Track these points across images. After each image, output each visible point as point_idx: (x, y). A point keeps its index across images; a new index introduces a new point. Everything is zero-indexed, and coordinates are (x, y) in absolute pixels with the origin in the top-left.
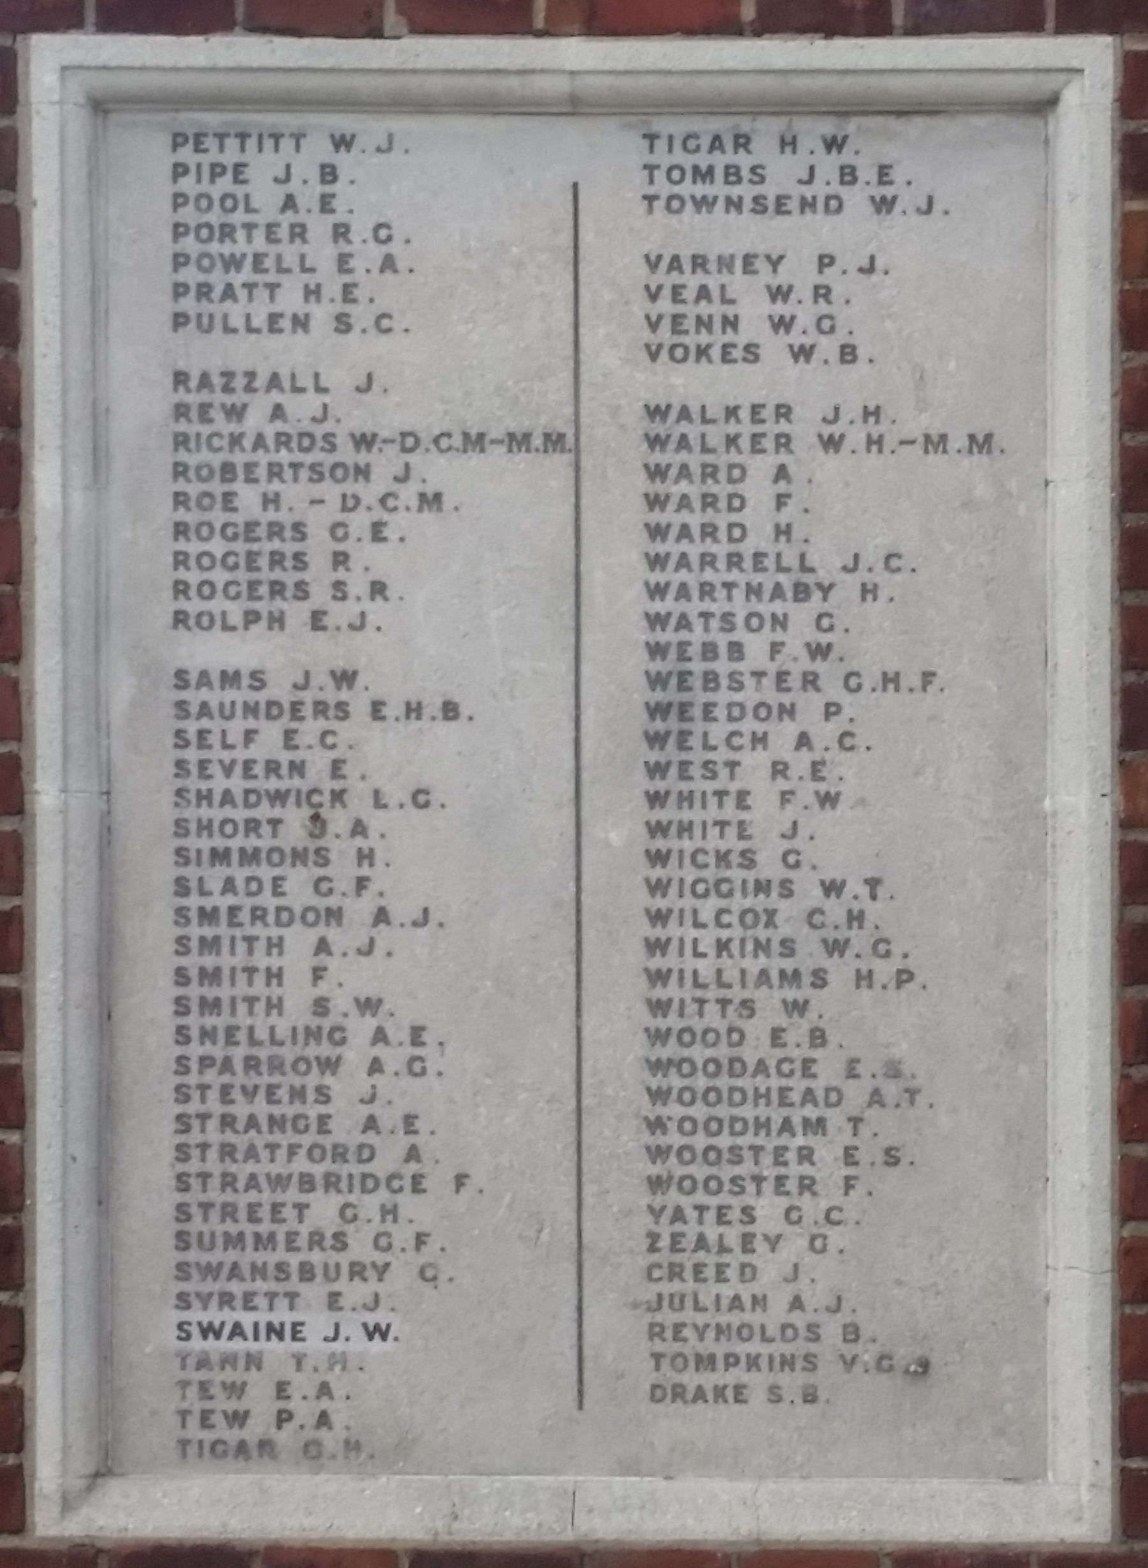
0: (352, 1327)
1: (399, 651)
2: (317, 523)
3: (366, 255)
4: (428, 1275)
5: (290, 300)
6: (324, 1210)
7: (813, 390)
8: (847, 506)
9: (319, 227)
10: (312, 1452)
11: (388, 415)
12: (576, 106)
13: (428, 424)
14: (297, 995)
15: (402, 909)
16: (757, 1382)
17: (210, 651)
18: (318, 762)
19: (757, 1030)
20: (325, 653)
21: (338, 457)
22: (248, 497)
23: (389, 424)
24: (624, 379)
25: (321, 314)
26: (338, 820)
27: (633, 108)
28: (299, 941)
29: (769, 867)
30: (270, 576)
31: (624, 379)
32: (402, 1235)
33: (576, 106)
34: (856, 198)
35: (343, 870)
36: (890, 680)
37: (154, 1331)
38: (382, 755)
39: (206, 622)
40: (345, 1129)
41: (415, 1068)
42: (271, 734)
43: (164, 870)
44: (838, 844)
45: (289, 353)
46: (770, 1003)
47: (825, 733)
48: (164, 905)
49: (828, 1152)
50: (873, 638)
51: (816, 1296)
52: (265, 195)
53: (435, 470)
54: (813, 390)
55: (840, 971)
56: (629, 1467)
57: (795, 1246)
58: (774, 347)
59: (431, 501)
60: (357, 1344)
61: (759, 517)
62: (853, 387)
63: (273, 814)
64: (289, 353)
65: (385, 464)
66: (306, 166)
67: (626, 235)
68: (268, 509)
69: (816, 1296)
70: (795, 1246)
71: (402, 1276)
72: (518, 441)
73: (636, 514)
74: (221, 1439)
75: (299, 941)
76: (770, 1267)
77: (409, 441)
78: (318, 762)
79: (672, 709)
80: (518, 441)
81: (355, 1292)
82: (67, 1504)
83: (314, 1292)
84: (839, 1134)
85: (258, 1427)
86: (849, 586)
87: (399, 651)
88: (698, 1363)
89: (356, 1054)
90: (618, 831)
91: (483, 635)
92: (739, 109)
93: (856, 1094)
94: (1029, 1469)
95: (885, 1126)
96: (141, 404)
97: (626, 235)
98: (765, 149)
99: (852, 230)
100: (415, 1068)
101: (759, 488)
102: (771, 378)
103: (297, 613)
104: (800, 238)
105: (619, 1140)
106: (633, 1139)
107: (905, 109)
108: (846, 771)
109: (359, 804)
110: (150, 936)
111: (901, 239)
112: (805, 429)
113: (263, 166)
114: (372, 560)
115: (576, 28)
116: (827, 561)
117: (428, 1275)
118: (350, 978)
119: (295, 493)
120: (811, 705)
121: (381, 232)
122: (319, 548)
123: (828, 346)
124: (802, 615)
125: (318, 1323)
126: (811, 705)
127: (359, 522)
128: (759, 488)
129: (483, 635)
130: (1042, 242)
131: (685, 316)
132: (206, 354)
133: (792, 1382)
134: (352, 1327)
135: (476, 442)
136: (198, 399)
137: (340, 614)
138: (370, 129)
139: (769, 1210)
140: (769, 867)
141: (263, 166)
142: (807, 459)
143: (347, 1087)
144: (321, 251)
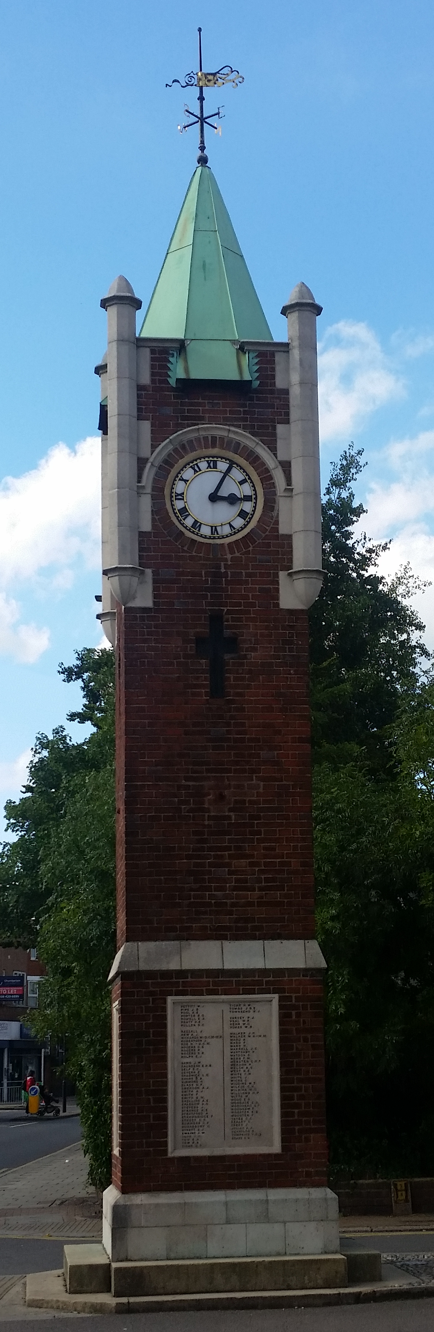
0: (201, 1132)
1: (205, 1060)
2: (196, 1046)
3: (201, 1018)
4: (208, 1126)
5: (193, 1023)
6: (198, 1120)
7: (247, 1031)
8: (251, 1043)
9: (196, 1015)
10: (197, 1147)
11: (204, 1035)
12: (223, 1002)
13: (208, 1036)
14: (195, 1096)
15: (206, 1087)
16: (243, 1137)
17: (185, 1060)
18: (197, 1072)
19: (243, 1099)
20: (197, 1060)
21: (199, 1039)
22: (189, 1044)
23: (204, 1035)
24: (228, 1030)
25: (197, 1024)
26: (199, 1078)
27: (229, 1002)
28: (195, 1091)
29: (244, 1081)
30: (191, 1052)
31: (228, 1030)
32: (206, 1122)
33: (223, 1002)
34: (252, 1011)
35: (199, 1083)
36: (256, 1061)
37: (180, 1133)
38: (203, 1070)
39: (185, 1057)
40: (200, 1111)
41: (207, 1104)
42: (191, 1069)
43: (181, 1084)
44: (251, 1079)
45: (194, 1028)
46: (244, 1096)
47: (249, 1067)
48: (181, 1088)
49: (250, 1111)
50: (254, 1057)
51: (249, 1128)
52: (191, 1012)
53: (209, 1040)
54: (247, 1031)
55: (251, 1092)
56: (230, 1147)
57: (247, 1122)
58: (243, 1027)
59: (208, 1044)
60: (201, 1134)
61: (242, 1044)
62: (252, 1030)
63: (192, 1077)
64: (194, 1028)
65: (203, 1040)
66: (195, 1009)
67: (228, 1015)
68: (191, 1045)
69: (249, 1128)
70: (247, 1122)
71: (206, 1127)
72: (217, 1037)
73: (230, 1044)
74: (187, 1145)
75: (195, 1091)
76: (244, 1124)
77: (206, 1037)
78: (197, 1072)
79: (233, 1065)
80: (217, 1037)
81: (201, 1129)
82: (172, 1153)
83: (196, 1129)
84: (251, 1110)
85: (191, 1143)
86: (251, 1051)
87: (205, 1060)
88: (237, 1135)
89: (201, 1103)
90: (228, 1078)
91: (213, 1057)
92: (239, 1002)
93: (253, 1106)
94: (271, 1145)
95: (256, 1109)
96: (178, 1034)
97: (228, 1015)
98: (242, 1006)
99: (251, 1014)
100: (207, 1104)
101: (242, 1041)
102: (243, 1030)
103: (194, 1056)
104: (246, 1015)
105: (228, 1110)
106: (230, 1111)
107: (205, 1002)
108: (251, 1071)
109: (201, 1076)
110: (179, 1090)
111: (256, 1015)
112: (247, 1035)
113: (190, 1009)
114: (201, 1050)
115: (144, 599)
116: (249, 1048)
117: (208, 1126)
118: (200, 1095)
119: (194, 1043)
120: (248, 1064)
121: (203, 1015)
122: (197, 1049)
123: (249, 1026)
124: (247, 1055)
125: (197, 1132)
126: (248, 1064)
127: (201, 1046)
128: (242, 1041)
129: (213, 1057)
130: (271, 1015)
131: (234, 1023)
132: (184, 1029)
133: (247, 1137)
134: (201, 1132)
135: (213, 1037)
136: (184, 1033)
137: (199, 1056)
138: (201, 1005)
139: (244, 1118)
140: (244, 1081)
141: (190, 1009)
142: (247, 1038)
143: (200, 1106)
144: (197, 1018)
